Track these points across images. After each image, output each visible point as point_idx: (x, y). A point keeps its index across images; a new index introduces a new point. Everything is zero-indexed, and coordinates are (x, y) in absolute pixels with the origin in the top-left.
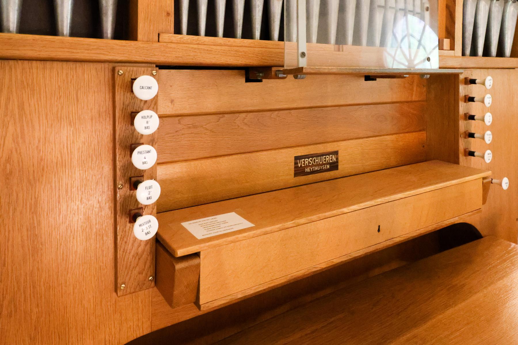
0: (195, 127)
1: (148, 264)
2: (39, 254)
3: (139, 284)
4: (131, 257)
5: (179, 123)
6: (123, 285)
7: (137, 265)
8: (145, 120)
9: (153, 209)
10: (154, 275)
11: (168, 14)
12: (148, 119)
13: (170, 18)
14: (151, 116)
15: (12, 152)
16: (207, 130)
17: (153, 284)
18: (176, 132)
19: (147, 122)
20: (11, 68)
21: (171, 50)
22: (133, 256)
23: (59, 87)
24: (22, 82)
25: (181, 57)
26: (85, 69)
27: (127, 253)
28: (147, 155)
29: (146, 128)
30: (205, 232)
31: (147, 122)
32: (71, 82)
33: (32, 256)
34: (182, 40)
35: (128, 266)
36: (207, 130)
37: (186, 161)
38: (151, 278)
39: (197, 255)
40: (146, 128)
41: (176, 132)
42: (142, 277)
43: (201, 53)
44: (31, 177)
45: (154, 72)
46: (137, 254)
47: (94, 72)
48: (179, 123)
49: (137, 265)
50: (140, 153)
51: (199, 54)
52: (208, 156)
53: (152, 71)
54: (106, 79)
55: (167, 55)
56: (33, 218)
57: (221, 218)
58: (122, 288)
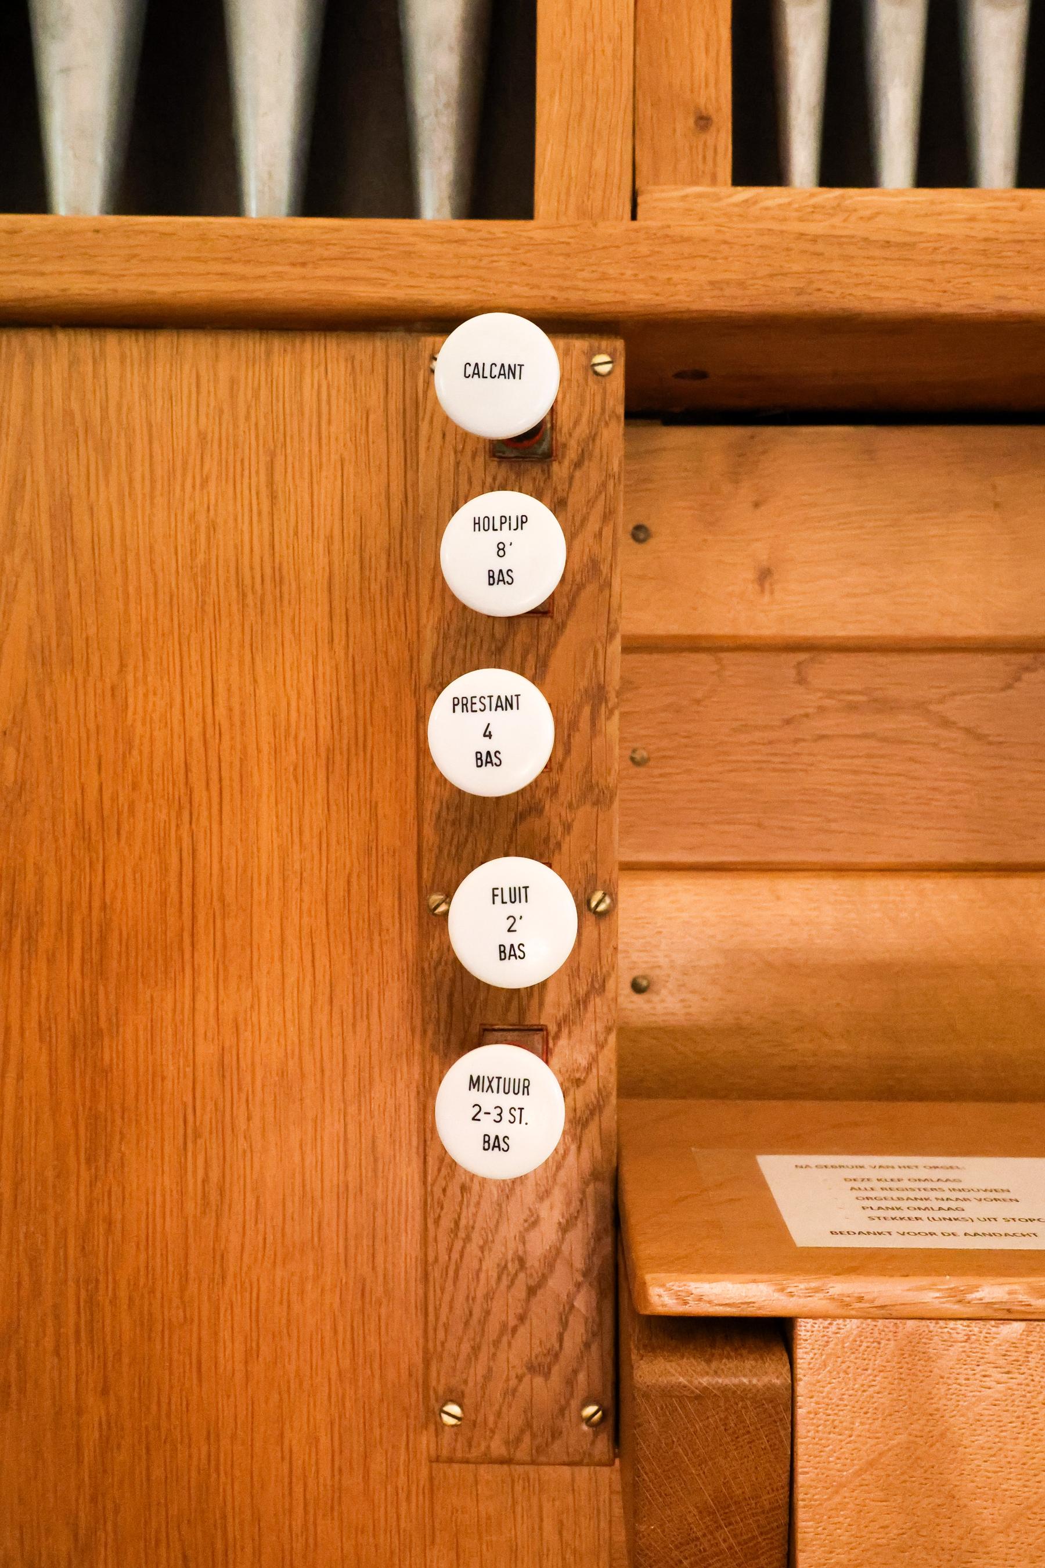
0: (885, 706)
1: (577, 1333)
2: (115, 1156)
3: (529, 1425)
4: (490, 1264)
5: (801, 681)
6: (454, 1409)
7: (522, 1318)
8: (492, 538)
9: (601, 1046)
10: (608, 1402)
11: (703, 122)
12: (505, 535)
13: (710, 138)
14: (523, 520)
15: (25, 702)
16: (946, 723)
17: (602, 1446)
18: (788, 722)
19: (501, 550)
20: (30, 360)
21: (687, 249)
22: (503, 1268)
23: (202, 437)
24: (68, 414)
25: (741, 284)
26: (302, 367)
27: (473, 1248)
28: (498, 719)
29: (496, 578)
30: (859, 1221)
31: (501, 550)
32: (247, 418)
33: (88, 1161)
34: (755, 210)
35: (477, 1312)
36: (946, 723)
37: (840, 870)
38: (590, 1410)
39: (775, 1333)
40: (496, 578)
41: (788, 722)
42: (544, 1391)
43: (848, 258)
44: (91, 816)
45: (598, 359)
46: (522, 1261)
47: (339, 372)
48: (801, 681)
49: (522, 1318)
50: (463, 704)
51: (836, 266)
52: (959, 858)
53: (592, 353)
54: (392, 407)
55: (663, 276)
56: (94, 995)
57: (980, 1171)
58: (448, 1420)
